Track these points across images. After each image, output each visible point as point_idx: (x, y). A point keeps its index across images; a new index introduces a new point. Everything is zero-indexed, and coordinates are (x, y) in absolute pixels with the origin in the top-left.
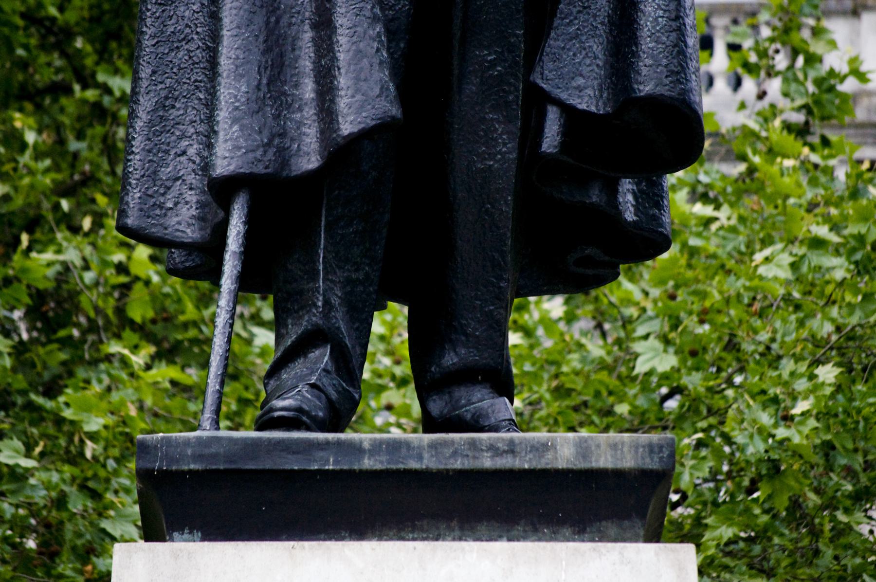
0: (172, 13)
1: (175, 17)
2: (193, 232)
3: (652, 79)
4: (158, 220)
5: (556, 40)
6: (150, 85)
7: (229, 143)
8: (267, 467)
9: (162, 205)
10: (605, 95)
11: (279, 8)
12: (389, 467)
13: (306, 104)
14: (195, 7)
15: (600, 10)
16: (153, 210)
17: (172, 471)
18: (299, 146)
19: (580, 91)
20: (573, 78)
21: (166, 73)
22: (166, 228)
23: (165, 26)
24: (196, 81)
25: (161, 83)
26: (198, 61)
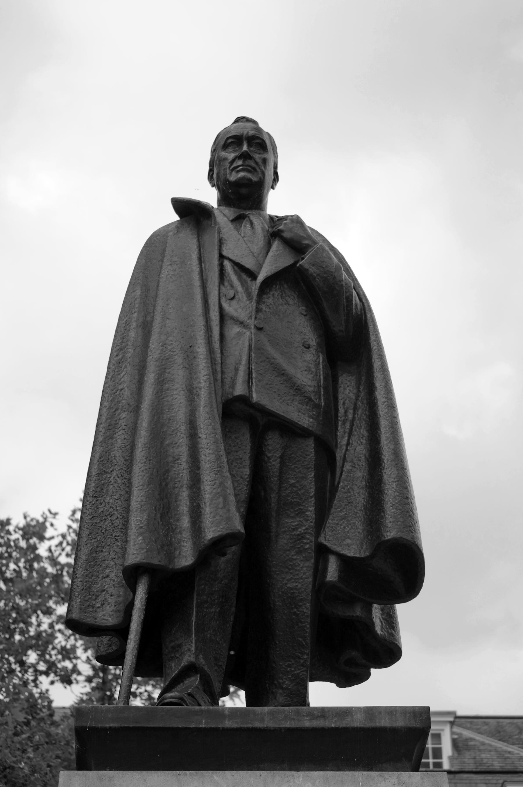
0: (102, 501)
1: (104, 503)
2: (113, 619)
3: (395, 529)
4: (91, 614)
5: (332, 520)
6: (88, 540)
7: (137, 546)
8: (161, 726)
9: (94, 606)
10: (365, 547)
11: (167, 478)
12: (242, 726)
13: (184, 530)
14: (116, 497)
15: (358, 503)
16: (88, 609)
17: (98, 728)
18: (180, 552)
19: (349, 547)
20: (344, 540)
21: (98, 533)
22: (96, 619)
23: (98, 508)
24: (116, 536)
25: (95, 539)
26: (117, 525)
